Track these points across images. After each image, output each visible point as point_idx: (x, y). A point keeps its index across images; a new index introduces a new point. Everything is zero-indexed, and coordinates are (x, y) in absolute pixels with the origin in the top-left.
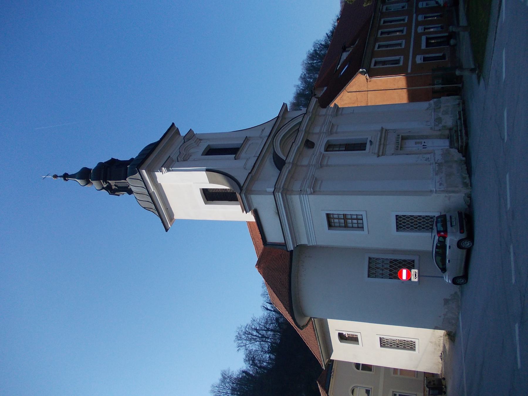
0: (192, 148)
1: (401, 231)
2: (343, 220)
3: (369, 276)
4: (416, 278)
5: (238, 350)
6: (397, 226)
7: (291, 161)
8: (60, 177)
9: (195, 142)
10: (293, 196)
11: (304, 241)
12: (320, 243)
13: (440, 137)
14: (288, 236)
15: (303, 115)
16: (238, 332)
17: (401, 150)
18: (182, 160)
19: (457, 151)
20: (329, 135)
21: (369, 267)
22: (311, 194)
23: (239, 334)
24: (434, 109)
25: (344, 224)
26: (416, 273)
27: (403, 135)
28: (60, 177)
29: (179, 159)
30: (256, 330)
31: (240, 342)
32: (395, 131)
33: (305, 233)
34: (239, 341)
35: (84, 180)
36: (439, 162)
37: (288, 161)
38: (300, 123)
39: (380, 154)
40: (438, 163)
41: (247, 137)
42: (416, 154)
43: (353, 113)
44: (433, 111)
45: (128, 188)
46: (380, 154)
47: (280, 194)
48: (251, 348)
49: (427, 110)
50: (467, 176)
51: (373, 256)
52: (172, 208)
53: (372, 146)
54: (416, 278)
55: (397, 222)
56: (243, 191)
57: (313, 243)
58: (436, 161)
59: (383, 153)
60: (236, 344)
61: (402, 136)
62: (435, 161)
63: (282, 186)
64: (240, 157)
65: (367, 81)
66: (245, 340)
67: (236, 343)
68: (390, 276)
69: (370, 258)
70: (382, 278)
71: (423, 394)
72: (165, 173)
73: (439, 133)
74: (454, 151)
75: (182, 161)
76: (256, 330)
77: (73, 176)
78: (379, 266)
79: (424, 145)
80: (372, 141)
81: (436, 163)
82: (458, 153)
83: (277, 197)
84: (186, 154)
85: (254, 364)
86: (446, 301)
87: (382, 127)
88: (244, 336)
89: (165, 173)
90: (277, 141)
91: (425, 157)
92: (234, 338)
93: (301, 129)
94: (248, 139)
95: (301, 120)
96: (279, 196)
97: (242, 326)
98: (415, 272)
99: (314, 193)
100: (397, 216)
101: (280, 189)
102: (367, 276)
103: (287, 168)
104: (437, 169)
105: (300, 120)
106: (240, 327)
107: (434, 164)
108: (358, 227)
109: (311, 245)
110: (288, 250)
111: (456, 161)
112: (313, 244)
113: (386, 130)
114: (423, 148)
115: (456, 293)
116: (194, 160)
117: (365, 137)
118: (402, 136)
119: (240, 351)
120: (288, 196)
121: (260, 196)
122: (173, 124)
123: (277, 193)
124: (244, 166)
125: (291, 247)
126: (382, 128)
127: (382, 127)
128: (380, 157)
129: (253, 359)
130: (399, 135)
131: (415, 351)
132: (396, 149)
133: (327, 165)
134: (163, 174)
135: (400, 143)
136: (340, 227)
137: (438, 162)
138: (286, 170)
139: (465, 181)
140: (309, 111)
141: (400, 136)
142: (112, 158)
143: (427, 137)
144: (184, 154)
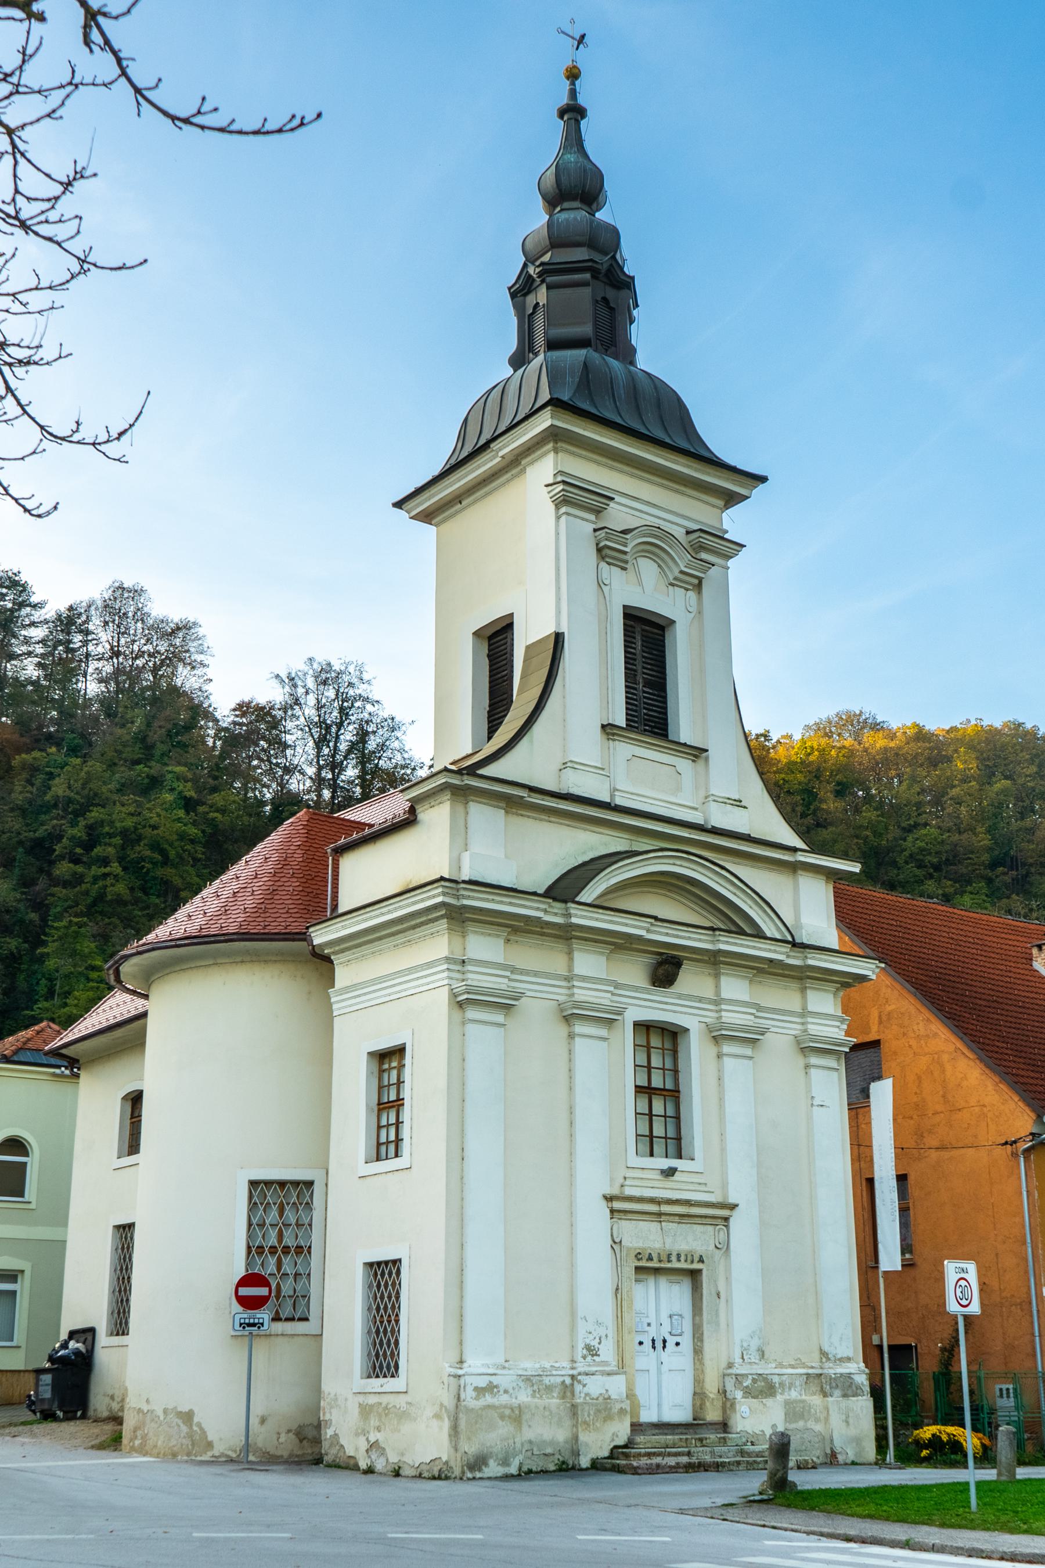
0: (659, 566)
1: (366, 1276)
2: (395, 1098)
3: (253, 1184)
4: (244, 1328)
5: (277, 676)
6: (379, 1264)
7: (574, 920)
8: (573, 93)
9: (682, 572)
10: (445, 939)
11: (344, 974)
12: (339, 1025)
13: (699, 1396)
14: (344, 928)
15: (790, 939)
16: (343, 668)
17: (638, 1269)
18: (602, 544)
19: (621, 1441)
20: (711, 1032)
21: (282, 1184)
22: (453, 995)
23: (339, 673)
24: (821, 1375)
25: (386, 1100)
26: (259, 1327)
27: (704, 1273)
28: (573, 93)
29: (602, 534)
30: (363, 735)
31: (311, 683)
32: (724, 1248)
33: (355, 982)
34: (313, 679)
35: (555, 186)
36: (578, 1388)
37: (572, 911)
38: (760, 935)
39: (617, 1205)
40: (572, 1385)
41: (707, 751)
42: (619, 1317)
43: (812, 1105)
44: (811, 1371)
45: (529, 352)
46: (617, 1205)
47: (440, 899)
48: (290, 725)
49: (821, 1353)
50: (513, 1470)
51: (318, 1189)
52: (688, 407)
53: (659, 1177)
54: (244, 1328)
55: (386, 1263)
56: (458, 776)
57: (339, 1003)
58: (579, 1377)
59: (619, 1211)
60: (298, 665)
61: (700, 1271)
62: (580, 1374)
63: (466, 902)
64: (614, 740)
65: (1006, 1143)
66: (318, 701)
67: (306, 668)
68: (258, 1247)
69: (310, 1184)
70: (250, 1225)
71: (22, 1368)
72: (549, 492)
73: (711, 1387)
74: (621, 1431)
75: (597, 544)
76: (363, 735)
77: (574, 140)
78: (290, 1216)
79: (665, 1341)
80: (677, 1176)
81: (573, 1377)
82: (612, 1446)
83: (429, 890)
84: (625, 553)
85: (233, 740)
86: (188, 1417)
87: (737, 1205)
88: (333, 697)
89: (549, 492)
90: (671, 861)
91: (599, 1343)
92: (321, 658)
93: (721, 938)
94: (696, 756)
95: (769, 934)
96: (434, 897)
97: (369, 682)
98: (262, 1324)
99: (460, 1004)
100: (400, 1260)
101: (458, 899)
102: (253, 1178)
103: (545, 911)
104: (547, 1381)
105: (769, 930)
106: (366, 676)
107: (571, 1372)
108: (379, 1145)
109: (333, 1000)
110: (311, 930)
111: (576, 1438)
112: (335, 1007)
113: (726, 1219)
114: (653, 1341)
115: (210, 1445)
116: (600, 584)
117: (698, 1154)
118: (700, 1271)
119: (275, 683)
120: (443, 924)
121: (448, 834)
122: (763, 479)
123: (440, 890)
124: (571, 761)
125: (321, 936)
126: (733, 1207)
127: (737, 1205)
128: (604, 1203)
129: (250, 738)
130: (701, 1260)
131: (107, 1336)
132: (639, 1253)
133: (571, 1036)
134: (547, 486)
135: (669, 1265)
136: (380, 1088)
137: (575, 1382)
138: (538, 909)
139: (492, 1462)
140: (809, 956)
141: (696, 1266)
142: (633, 278)
143: (698, 1351)
144: (626, 546)
